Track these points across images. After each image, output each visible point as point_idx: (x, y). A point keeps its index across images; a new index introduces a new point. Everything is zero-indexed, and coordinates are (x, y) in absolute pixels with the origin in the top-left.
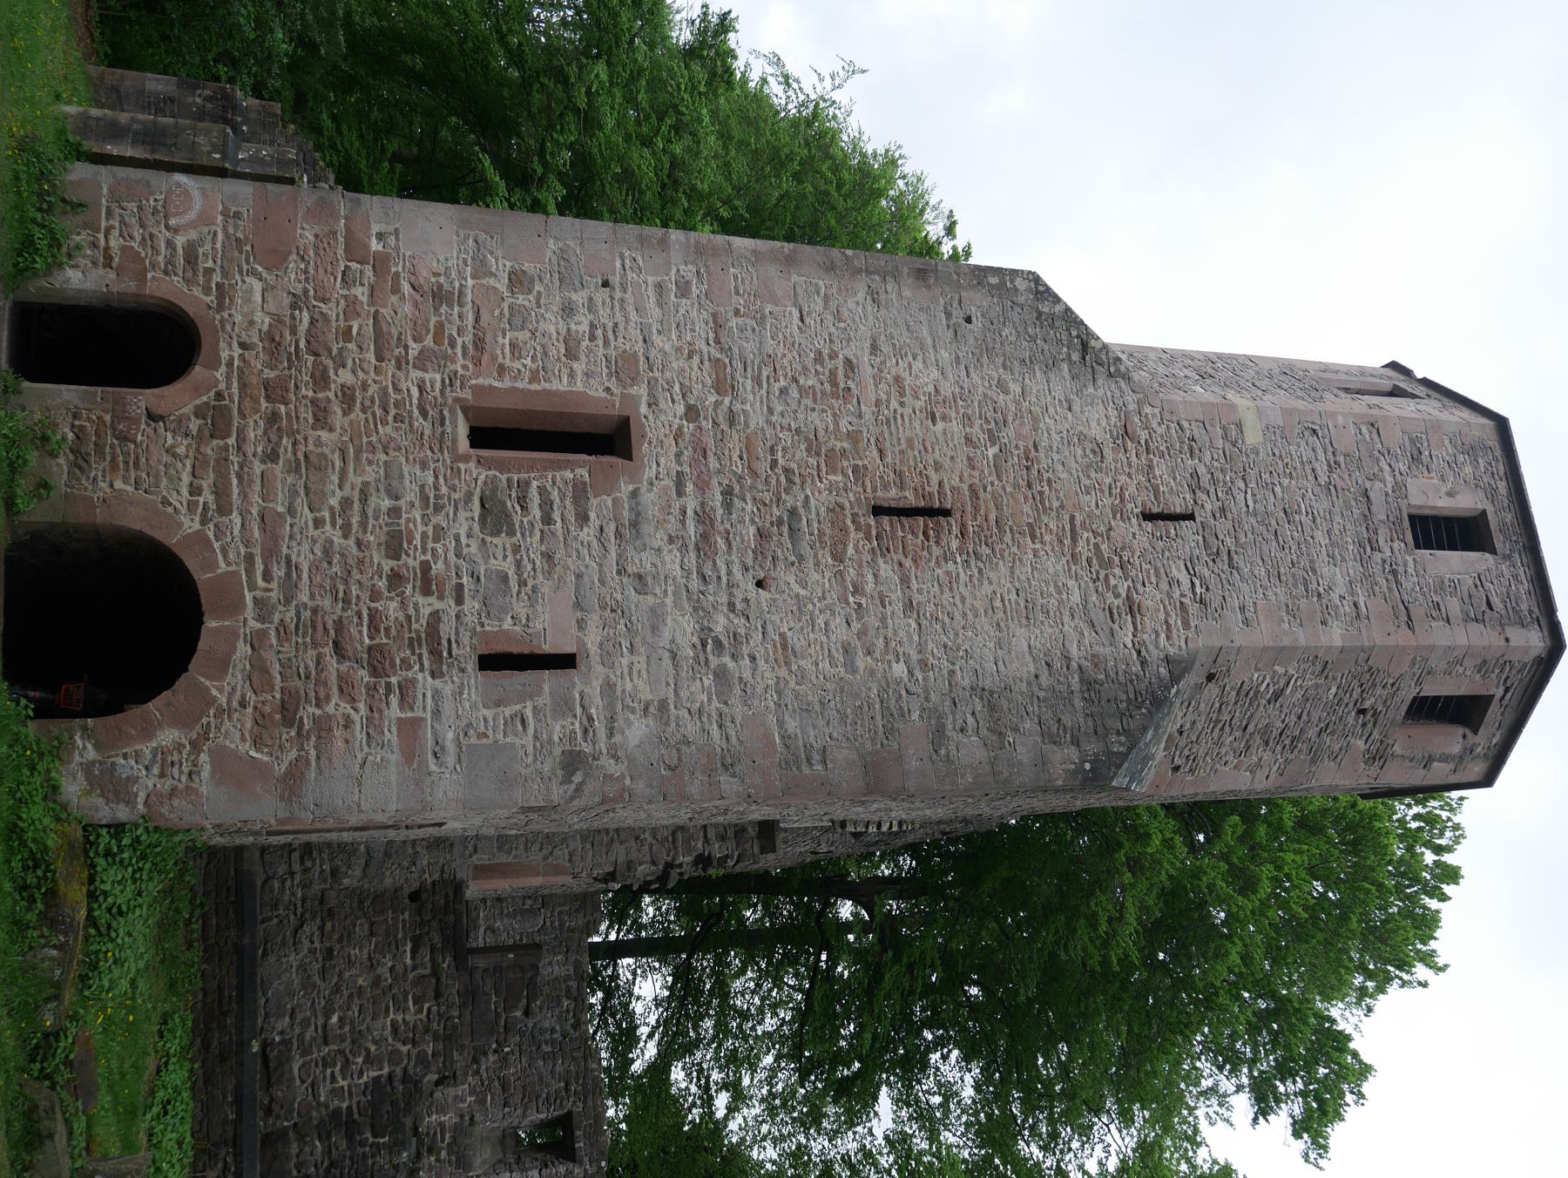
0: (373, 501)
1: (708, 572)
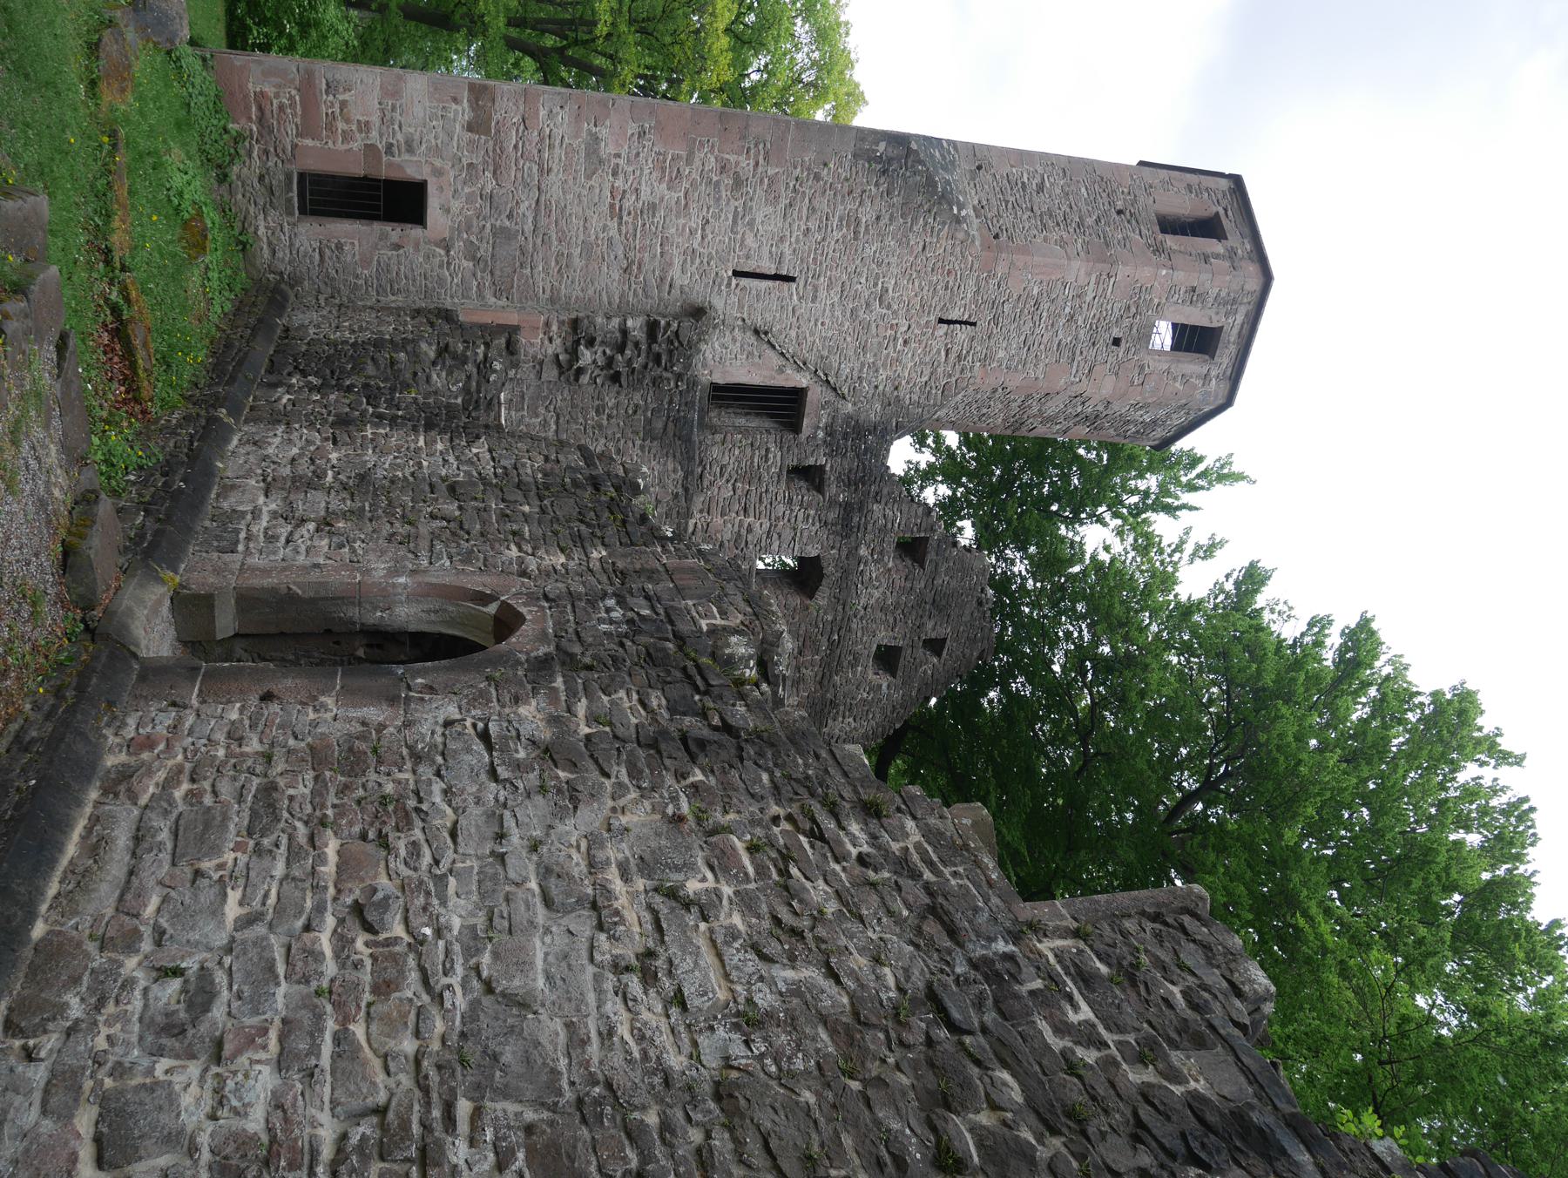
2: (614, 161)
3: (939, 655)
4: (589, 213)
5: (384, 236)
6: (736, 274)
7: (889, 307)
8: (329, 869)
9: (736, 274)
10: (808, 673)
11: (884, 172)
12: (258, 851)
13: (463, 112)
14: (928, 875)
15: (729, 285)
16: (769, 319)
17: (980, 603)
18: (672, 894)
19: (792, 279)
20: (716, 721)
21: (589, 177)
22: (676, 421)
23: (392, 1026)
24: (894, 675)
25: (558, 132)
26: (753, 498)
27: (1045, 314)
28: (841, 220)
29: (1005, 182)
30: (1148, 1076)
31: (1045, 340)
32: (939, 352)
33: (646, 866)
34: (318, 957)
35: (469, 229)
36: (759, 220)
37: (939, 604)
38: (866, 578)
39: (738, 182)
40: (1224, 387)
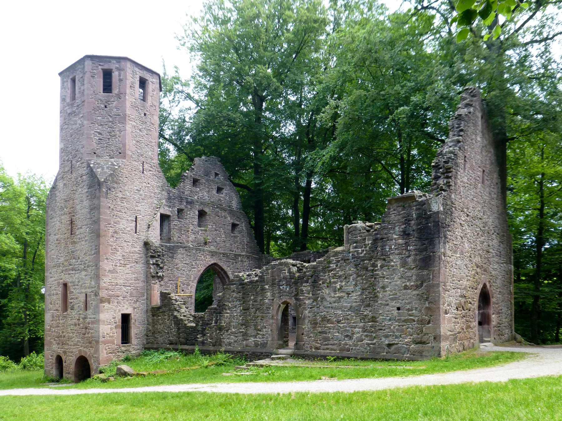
0: (72, 328)
1: (77, 269)
2: (113, 266)
3: (218, 174)
4: (125, 273)
5: (134, 324)
6: (136, 233)
7: (141, 189)
8: (332, 325)
9: (136, 233)
10: (223, 214)
12: (329, 333)
13: (106, 305)
14: (340, 259)
15: (138, 235)
16: (145, 224)
17: (206, 161)
18: (339, 289)
19: (136, 217)
20: (310, 277)
21: (117, 273)
22: (170, 250)
24: (223, 189)
25: (109, 281)
26: (185, 229)
27: (140, 139)
28: (122, 203)
29: (99, 145)
30: (368, 247)
31: (146, 139)
32: (150, 173)
33: (335, 291)
34: (343, 326)
35: (130, 303)
36: (124, 227)
37: (207, 174)
38: (202, 197)
39: (116, 232)
40: (155, 75)
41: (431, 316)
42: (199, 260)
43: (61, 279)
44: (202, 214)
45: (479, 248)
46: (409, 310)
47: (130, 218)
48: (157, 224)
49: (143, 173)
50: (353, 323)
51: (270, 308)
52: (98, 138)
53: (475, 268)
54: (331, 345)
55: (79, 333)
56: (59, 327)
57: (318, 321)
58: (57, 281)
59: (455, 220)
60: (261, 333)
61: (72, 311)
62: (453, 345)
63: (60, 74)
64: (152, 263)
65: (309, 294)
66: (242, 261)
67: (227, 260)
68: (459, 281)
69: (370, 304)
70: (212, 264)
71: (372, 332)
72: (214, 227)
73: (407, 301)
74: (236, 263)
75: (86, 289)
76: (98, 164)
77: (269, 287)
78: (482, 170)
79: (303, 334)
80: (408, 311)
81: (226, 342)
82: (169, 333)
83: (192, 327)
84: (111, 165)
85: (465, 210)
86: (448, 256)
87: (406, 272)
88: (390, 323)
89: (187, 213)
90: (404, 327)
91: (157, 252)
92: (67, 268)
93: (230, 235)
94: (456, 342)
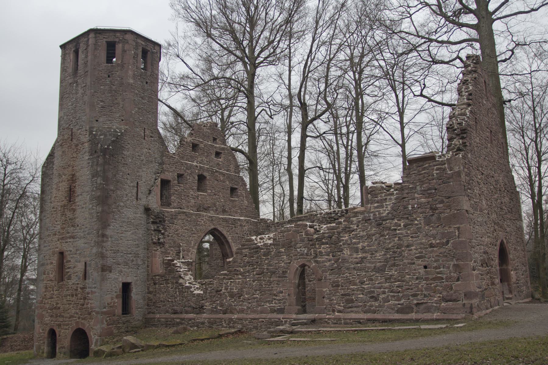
0: (68, 299)
8: (356, 287)
11: (113, 156)
19: (138, 182)
23: (377, 279)
29: (102, 113)
34: (368, 287)
41: (460, 273)
42: (199, 225)
43: (57, 248)
44: (201, 178)
45: (494, 205)
46: (436, 268)
47: (132, 185)
48: (157, 190)
49: (144, 139)
50: (378, 284)
51: (286, 272)
52: (100, 106)
53: (493, 225)
54: (355, 307)
55: (75, 304)
56: (52, 298)
57: (340, 283)
58: (51, 250)
59: (473, 179)
60: (278, 298)
61: (69, 281)
62: (482, 302)
63: (63, 47)
64: (153, 229)
65: (329, 255)
66: (241, 225)
67: (227, 225)
68: (482, 238)
69: (395, 263)
70: (212, 229)
71: (399, 292)
72: (213, 191)
73: (433, 259)
74: (235, 227)
75: (85, 257)
76: (100, 131)
77: (284, 250)
78: (490, 131)
79: (324, 298)
80: (436, 269)
81: (238, 309)
82: (173, 302)
83: (199, 295)
84: (113, 132)
85: (480, 169)
86: (471, 214)
87: (431, 230)
88: (417, 282)
89: (187, 178)
90: (433, 285)
91: (159, 218)
92: (64, 236)
93: (229, 199)
94: (484, 299)
